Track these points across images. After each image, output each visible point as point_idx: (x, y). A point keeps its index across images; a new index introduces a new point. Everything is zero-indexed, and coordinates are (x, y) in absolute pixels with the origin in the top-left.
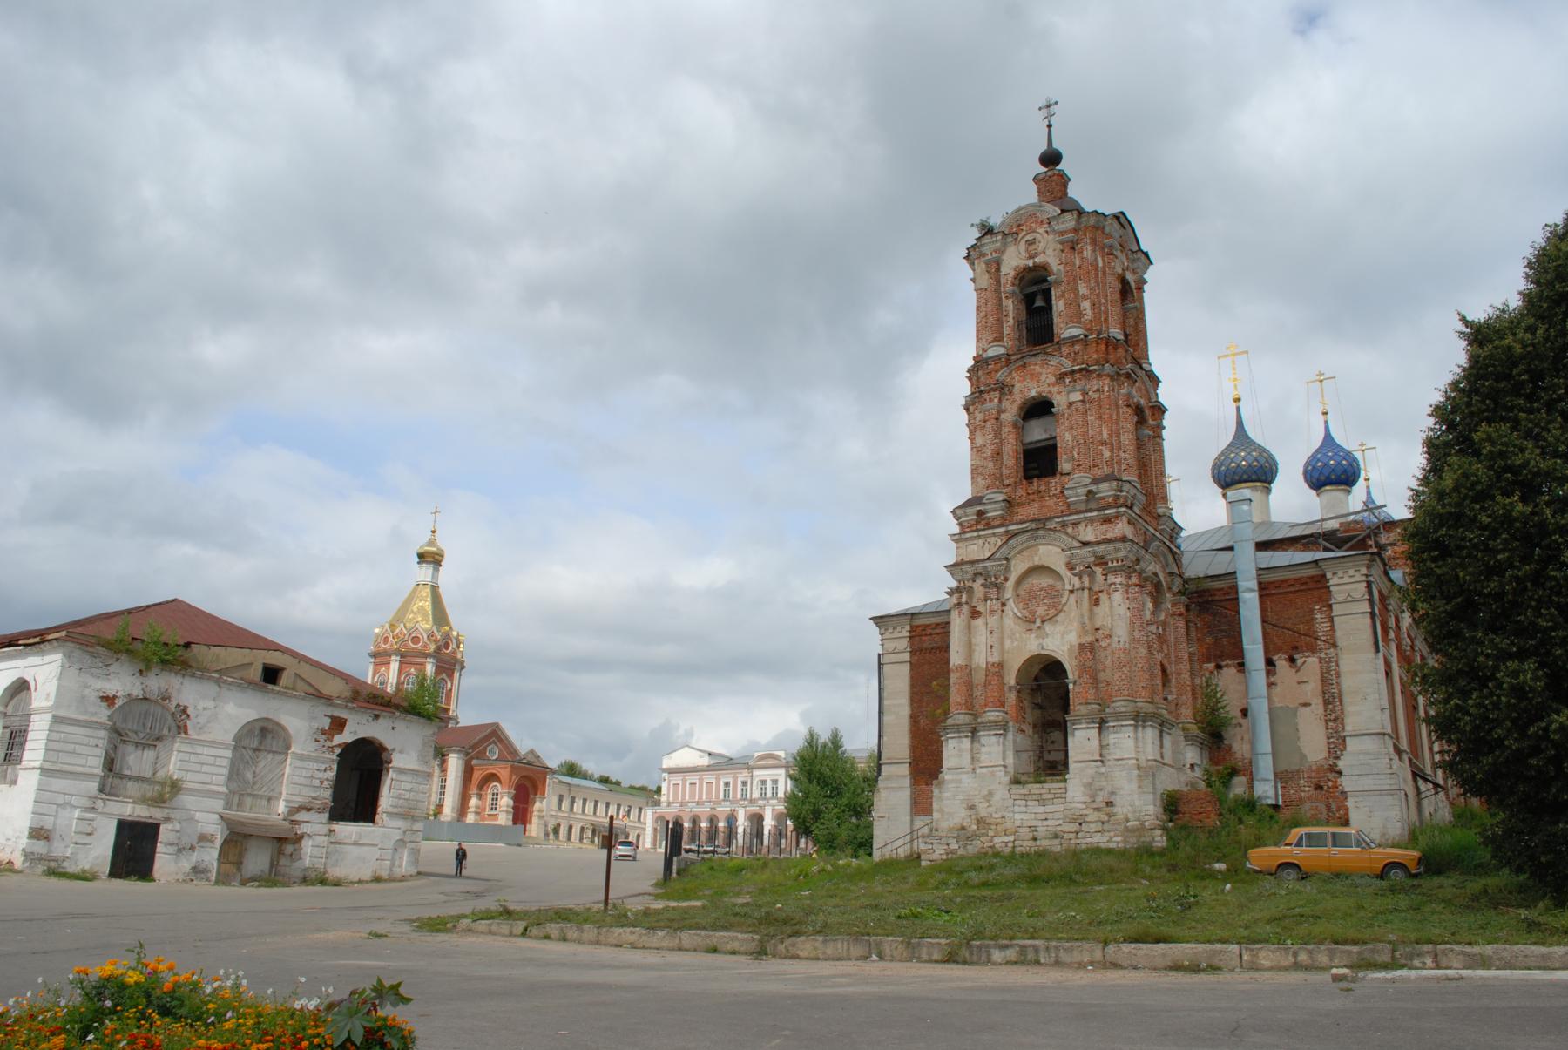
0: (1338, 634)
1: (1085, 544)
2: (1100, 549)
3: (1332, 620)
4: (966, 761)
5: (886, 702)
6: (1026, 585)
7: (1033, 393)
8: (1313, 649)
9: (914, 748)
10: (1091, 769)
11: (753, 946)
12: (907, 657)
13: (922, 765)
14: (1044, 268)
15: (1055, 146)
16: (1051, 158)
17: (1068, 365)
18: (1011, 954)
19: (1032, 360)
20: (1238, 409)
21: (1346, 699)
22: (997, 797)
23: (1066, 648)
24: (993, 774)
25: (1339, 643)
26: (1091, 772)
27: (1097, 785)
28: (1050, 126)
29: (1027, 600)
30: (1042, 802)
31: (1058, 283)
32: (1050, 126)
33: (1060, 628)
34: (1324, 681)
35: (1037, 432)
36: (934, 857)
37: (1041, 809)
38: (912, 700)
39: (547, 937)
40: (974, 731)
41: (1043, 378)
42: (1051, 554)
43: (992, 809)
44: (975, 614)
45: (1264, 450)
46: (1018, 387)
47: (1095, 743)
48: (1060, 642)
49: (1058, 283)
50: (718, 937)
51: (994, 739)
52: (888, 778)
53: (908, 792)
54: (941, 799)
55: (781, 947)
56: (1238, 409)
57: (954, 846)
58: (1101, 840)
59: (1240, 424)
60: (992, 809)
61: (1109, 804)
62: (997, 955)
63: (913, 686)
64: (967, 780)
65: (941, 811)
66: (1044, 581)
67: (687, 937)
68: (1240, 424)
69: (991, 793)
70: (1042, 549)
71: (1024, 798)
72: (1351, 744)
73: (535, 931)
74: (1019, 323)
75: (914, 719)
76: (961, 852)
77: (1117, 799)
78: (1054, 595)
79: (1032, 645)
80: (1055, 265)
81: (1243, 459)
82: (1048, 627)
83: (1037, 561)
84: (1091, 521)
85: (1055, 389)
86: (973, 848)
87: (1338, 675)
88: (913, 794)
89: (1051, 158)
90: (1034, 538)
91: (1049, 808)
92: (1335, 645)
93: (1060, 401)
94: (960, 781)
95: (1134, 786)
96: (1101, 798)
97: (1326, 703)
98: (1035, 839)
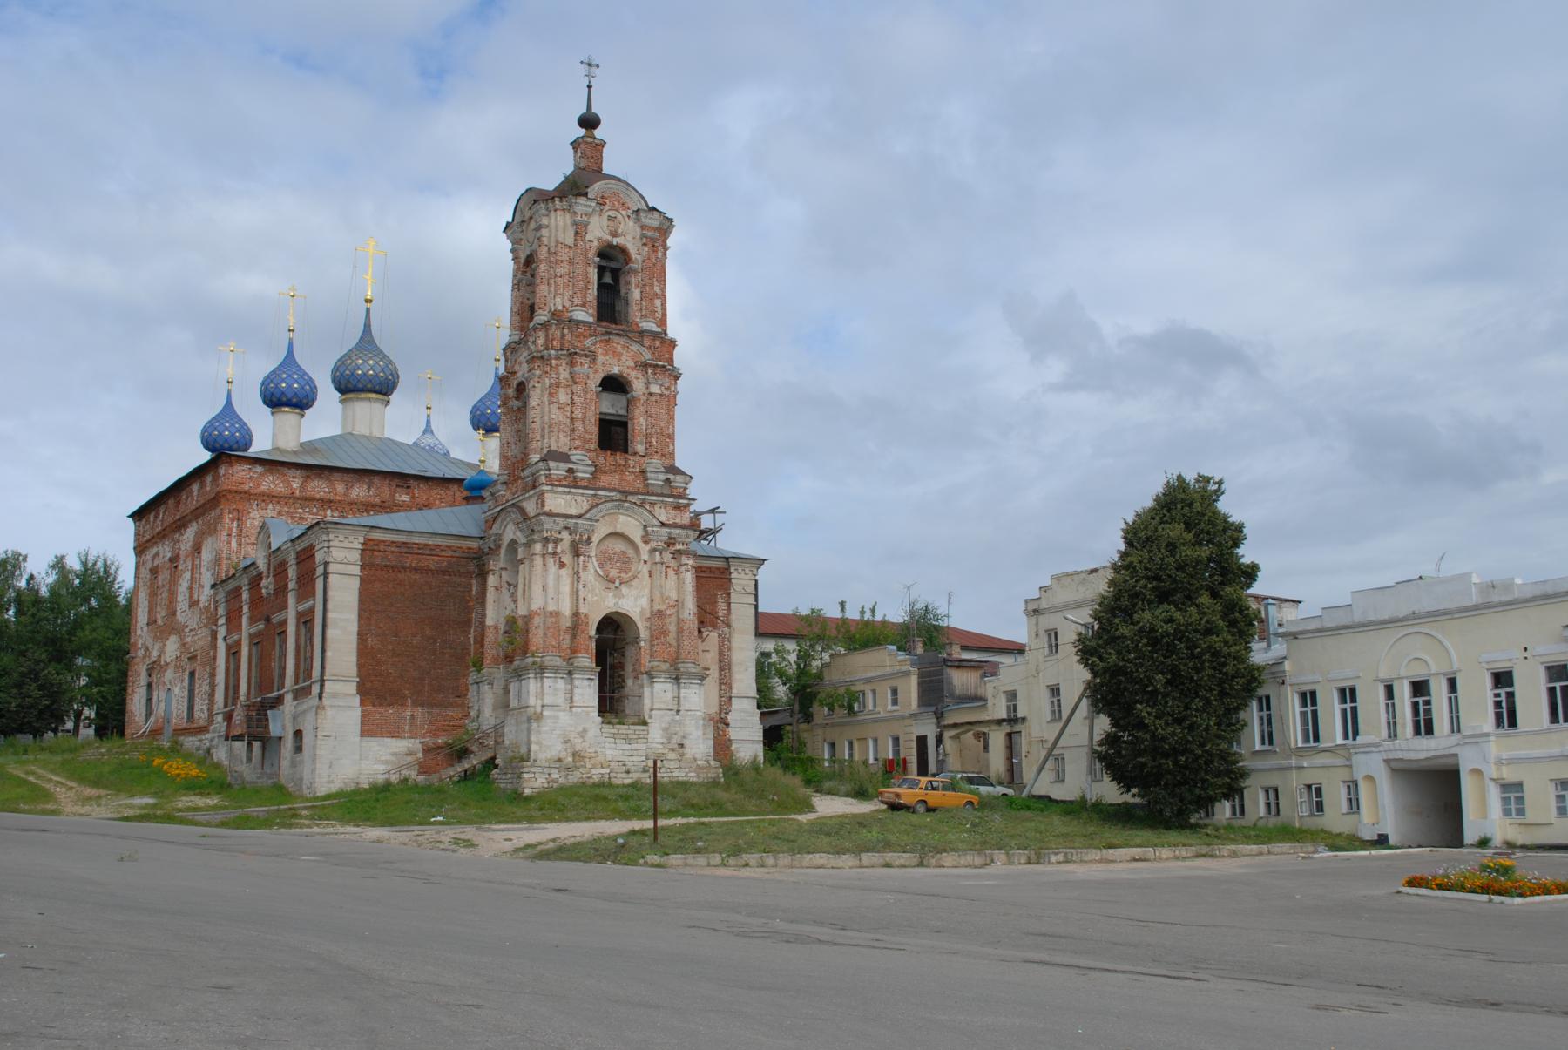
0: (733, 617)
1: (663, 524)
2: (676, 531)
3: (729, 604)
4: (561, 699)
5: (330, 615)
6: (603, 548)
7: (616, 370)
8: (715, 627)
9: (360, 666)
10: (669, 717)
11: (916, 861)
12: (357, 570)
13: (368, 685)
14: (624, 251)
15: (595, 110)
16: (589, 122)
17: (647, 356)
18: (1061, 857)
19: (616, 339)
20: (368, 310)
21: (735, 669)
22: (591, 734)
23: (638, 610)
24: (588, 714)
25: (734, 624)
26: (667, 719)
27: (673, 730)
28: (589, 87)
29: (604, 560)
30: (628, 740)
31: (636, 272)
32: (589, 87)
33: (634, 592)
34: (721, 653)
35: (611, 405)
36: (537, 785)
37: (627, 747)
38: (360, 617)
39: (747, 865)
40: (570, 673)
41: (624, 358)
42: (630, 524)
43: (586, 745)
44: (562, 565)
45: (391, 362)
46: (601, 359)
47: (669, 695)
48: (633, 603)
49: (636, 272)
50: (889, 856)
51: (586, 683)
52: (335, 695)
53: (358, 712)
54: (539, 732)
55: (933, 861)
56: (368, 310)
57: (555, 776)
58: (679, 775)
59: (367, 326)
60: (586, 745)
61: (682, 746)
62: (1053, 859)
63: (361, 601)
64: (564, 718)
65: (539, 743)
66: (618, 546)
67: (866, 858)
68: (367, 326)
69: (585, 731)
70: (622, 518)
71: (614, 736)
72: (736, 704)
73: (732, 861)
74: (627, 303)
75: (362, 637)
76: (561, 781)
77: (687, 742)
78: (625, 562)
79: (600, 603)
80: (633, 251)
81: (367, 367)
82: (624, 589)
83: (619, 529)
84: (665, 504)
85: (633, 374)
86: (574, 778)
87: (729, 649)
88: (363, 716)
89: (589, 122)
90: (618, 507)
91: (635, 746)
92: (729, 625)
93: (638, 386)
94: (557, 718)
95: (700, 733)
96: (675, 740)
97: (721, 669)
98: (628, 772)
